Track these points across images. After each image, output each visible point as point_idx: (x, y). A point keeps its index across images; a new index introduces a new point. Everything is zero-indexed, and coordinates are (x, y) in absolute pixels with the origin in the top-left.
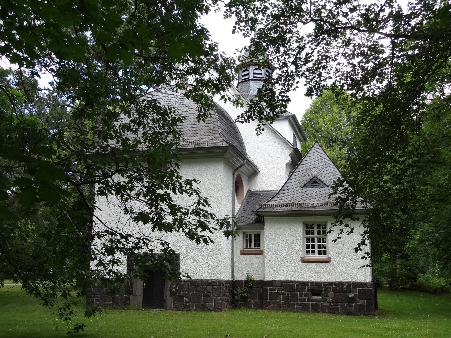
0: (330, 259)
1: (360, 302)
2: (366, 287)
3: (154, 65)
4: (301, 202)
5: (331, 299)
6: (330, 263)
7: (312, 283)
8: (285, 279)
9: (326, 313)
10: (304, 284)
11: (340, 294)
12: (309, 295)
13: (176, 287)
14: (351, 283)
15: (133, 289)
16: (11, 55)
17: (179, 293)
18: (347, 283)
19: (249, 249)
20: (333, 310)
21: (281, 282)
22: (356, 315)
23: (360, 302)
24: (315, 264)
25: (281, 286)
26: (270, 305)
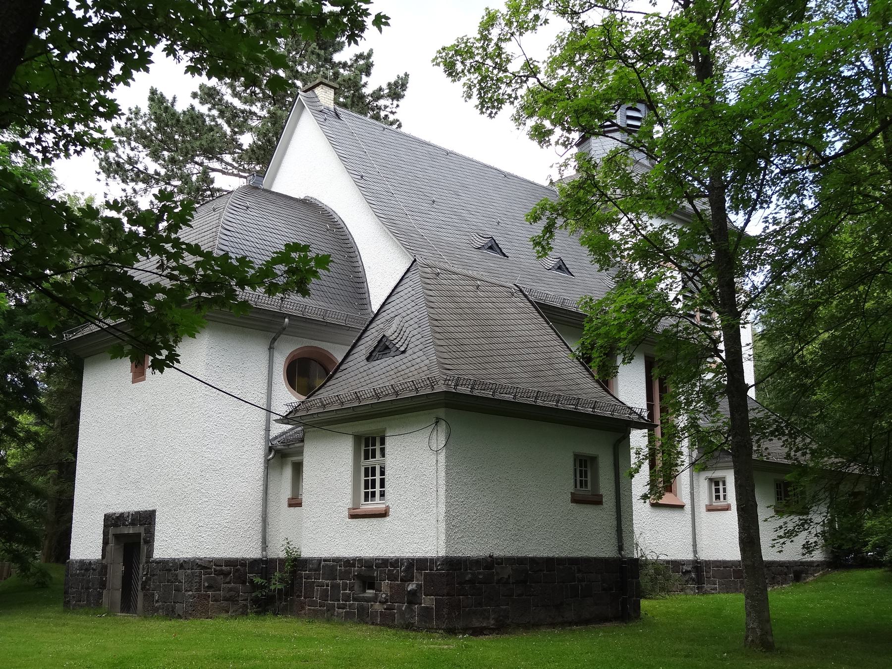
0: (387, 508)
1: (428, 601)
2: (435, 569)
3: (710, 370)
4: (392, 382)
5: (384, 596)
6: (388, 519)
7: (360, 560)
8: (325, 554)
9: (377, 624)
10: (349, 563)
11: (398, 585)
12: (356, 587)
13: (147, 574)
14: (413, 559)
15: (106, 578)
16: (139, 48)
17: (150, 585)
18: (408, 559)
19: (688, 507)
20: (387, 621)
21: (320, 560)
22: (418, 630)
23: (428, 601)
24: (367, 520)
25: (318, 569)
26: (303, 608)
